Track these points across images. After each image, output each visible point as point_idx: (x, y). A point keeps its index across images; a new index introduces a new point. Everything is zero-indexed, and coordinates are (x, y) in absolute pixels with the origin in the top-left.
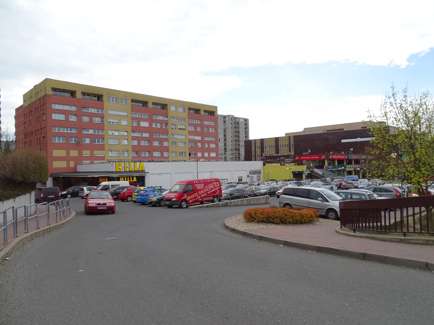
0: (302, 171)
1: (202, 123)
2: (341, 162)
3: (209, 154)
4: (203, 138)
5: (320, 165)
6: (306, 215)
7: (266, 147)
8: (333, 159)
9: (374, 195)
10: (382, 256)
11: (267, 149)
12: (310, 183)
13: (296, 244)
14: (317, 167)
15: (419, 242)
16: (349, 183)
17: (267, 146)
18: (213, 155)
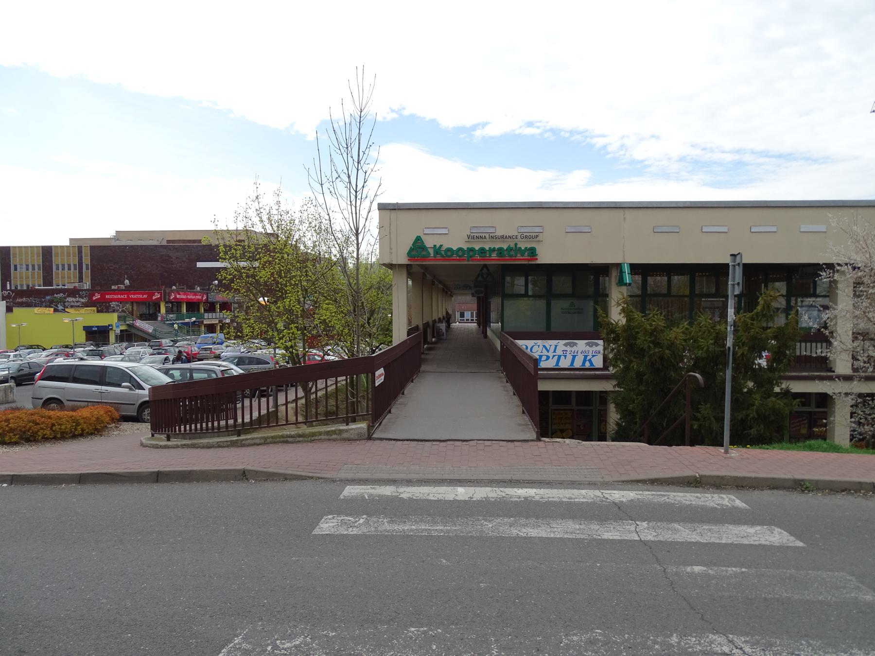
0: (107, 324)
2: (193, 307)
5: (149, 312)
6: (83, 418)
7: (16, 267)
8: (176, 301)
9: (232, 370)
10: (184, 471)
11: (20, 272)
12: (123, 351)
13: (37, 476)
14: (143, 317)
15: (255, 442)
16: (206, 349)
17: (21, 265)
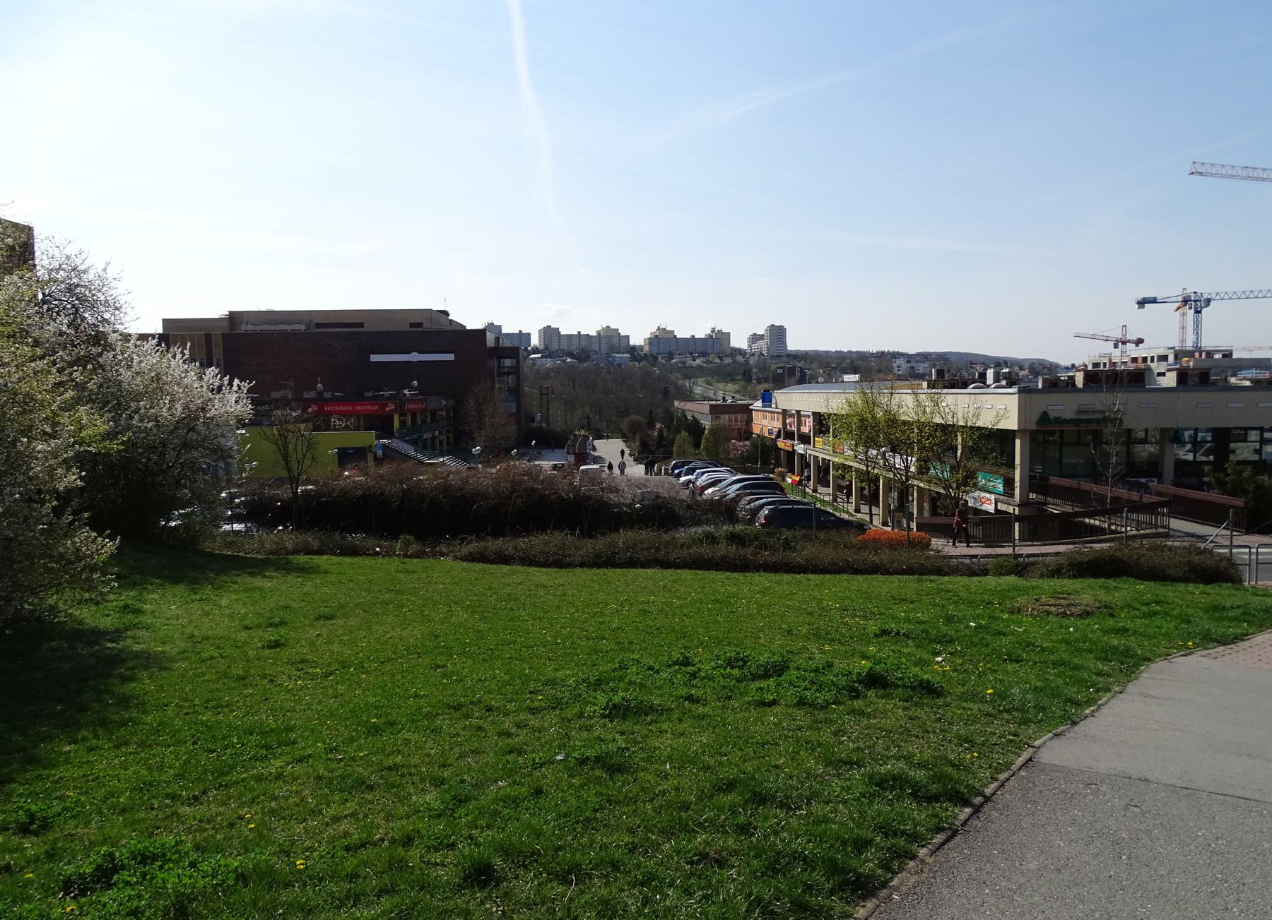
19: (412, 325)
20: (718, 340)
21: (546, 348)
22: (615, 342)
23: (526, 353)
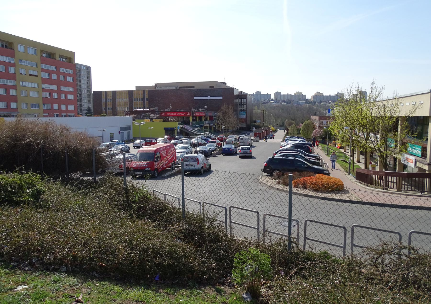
1: (58, 69)
3: (67, 107)
4: (59, 88)
18: (71, 107)
19: (210, 87)
20: (340, 96)
21: (276, 99)
22: (301, 97)
23: (269, 101)
